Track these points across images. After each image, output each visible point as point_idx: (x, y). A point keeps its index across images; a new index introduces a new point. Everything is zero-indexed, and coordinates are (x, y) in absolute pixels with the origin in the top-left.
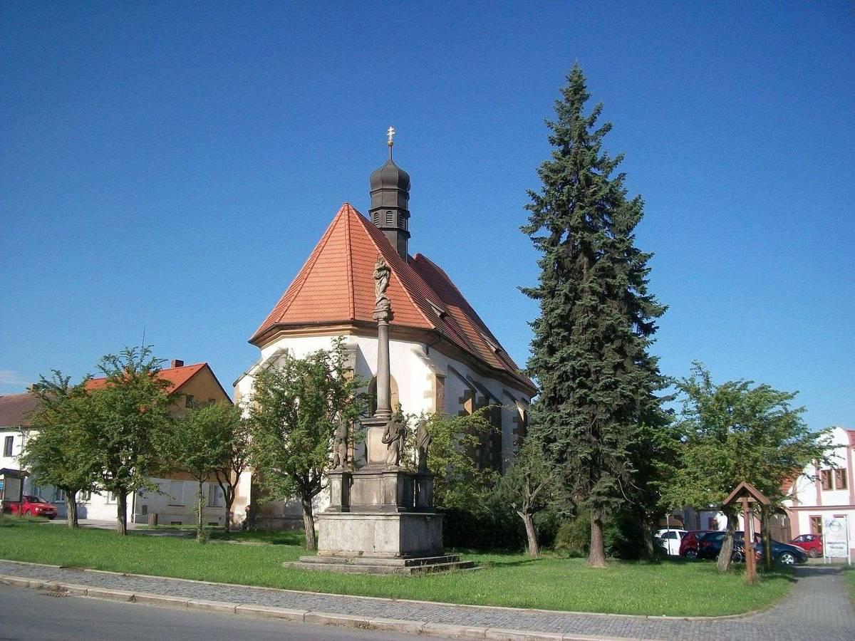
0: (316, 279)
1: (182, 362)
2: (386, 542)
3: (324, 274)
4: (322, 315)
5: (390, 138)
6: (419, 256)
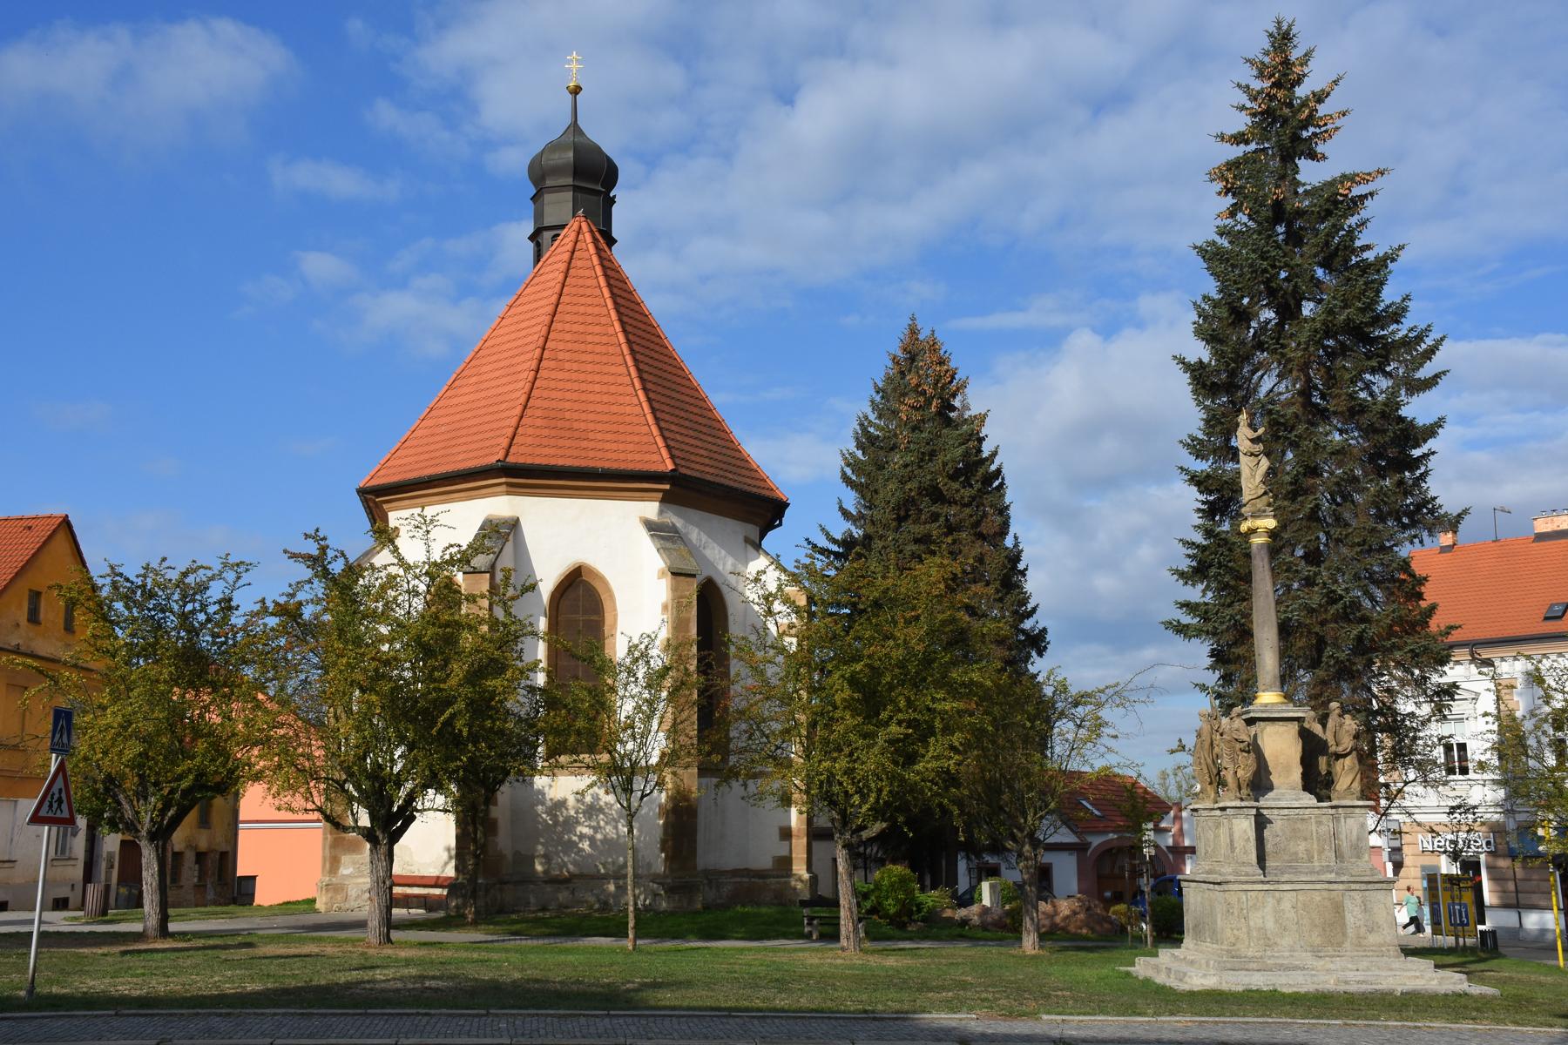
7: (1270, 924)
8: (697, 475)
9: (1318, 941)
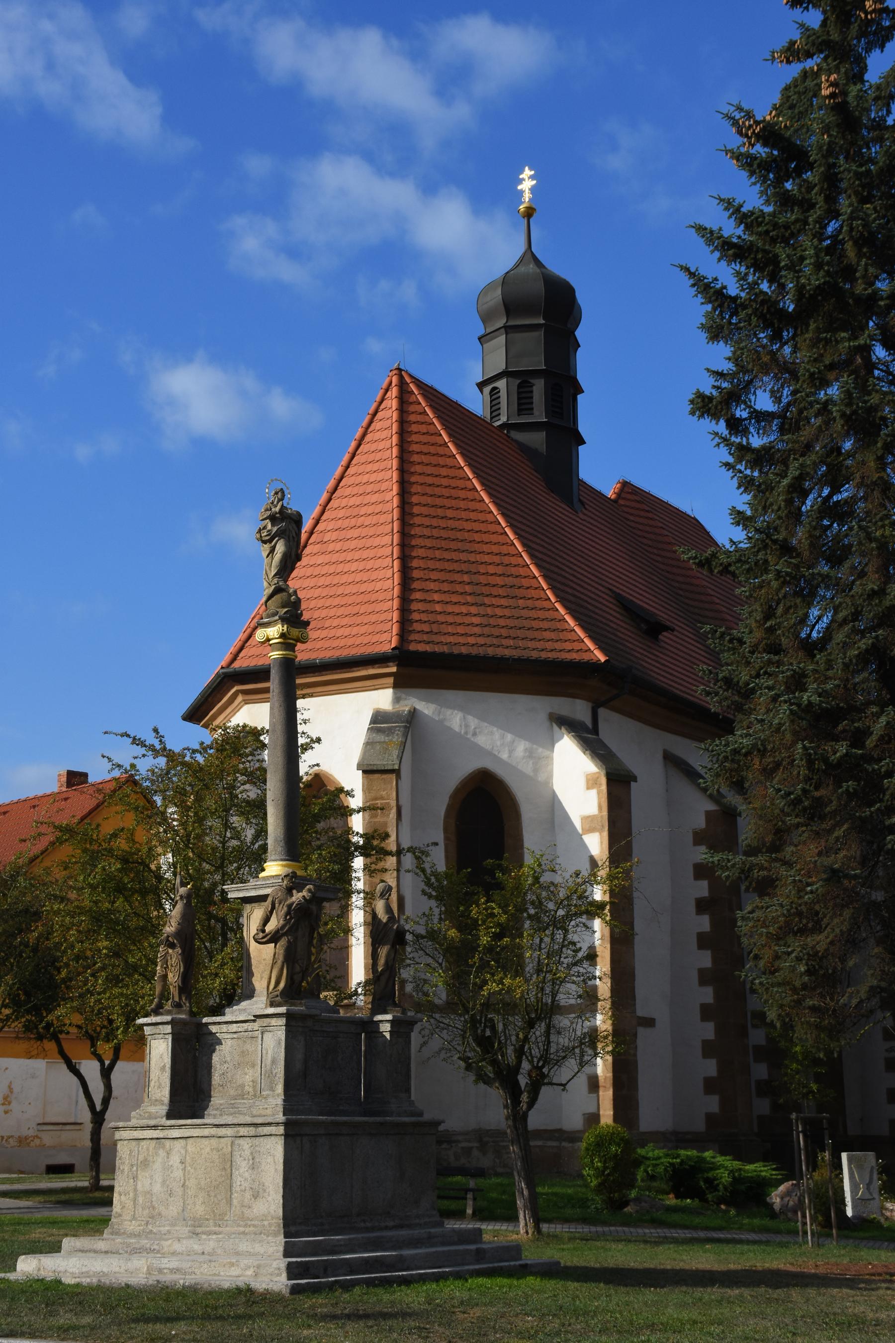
0: (320, 559)
1: (85, 775)
2: (256, 1196)
3: (338, 546)
4: (327, 644)
5: (527, 196)
6: (625, 486)
7: (157, 1188)
8: (446, 649)
9: (199, 1210)
